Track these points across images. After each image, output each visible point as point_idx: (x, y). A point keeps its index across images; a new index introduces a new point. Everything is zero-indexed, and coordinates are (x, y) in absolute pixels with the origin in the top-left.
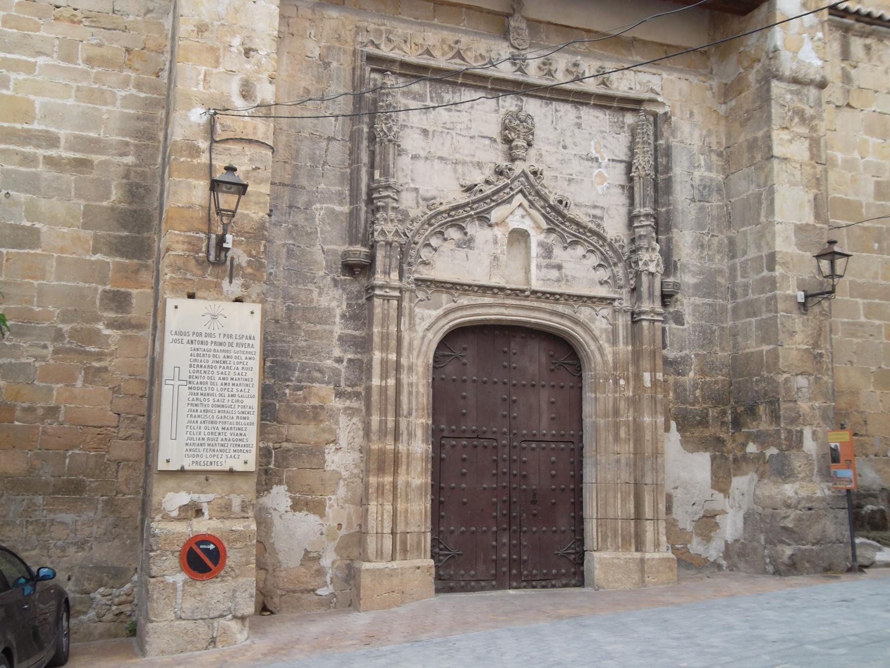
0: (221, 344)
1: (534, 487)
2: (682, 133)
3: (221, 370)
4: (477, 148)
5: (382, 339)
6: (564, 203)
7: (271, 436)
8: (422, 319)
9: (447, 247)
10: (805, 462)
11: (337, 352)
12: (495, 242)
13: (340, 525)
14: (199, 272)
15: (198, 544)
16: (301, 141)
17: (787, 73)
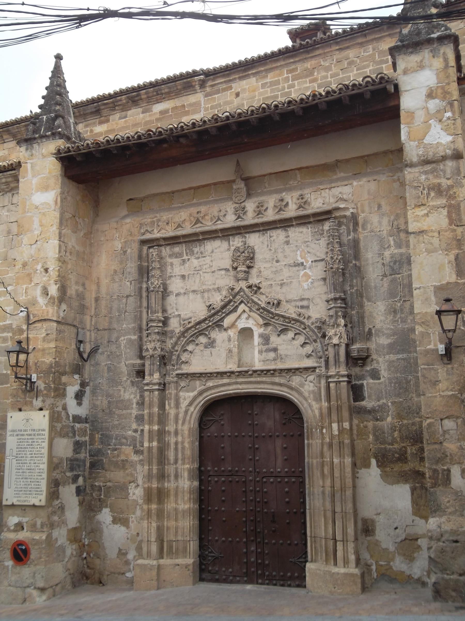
0: (30, 435)
1: (273, 510)
2: (372, 224)
3: (30, 449)
4: (217, 278)
5: (150, 417)
6: (272, 303)
7: (102, 479)
8: (185, 399)
9: (198, 350)
10: (454, 498)
11: (134, 426)
12: (229, 340)
13: (138, 534)
14: (23, 397)
15: (18, 545)
16: (113, 302)
17: (415, 159)
